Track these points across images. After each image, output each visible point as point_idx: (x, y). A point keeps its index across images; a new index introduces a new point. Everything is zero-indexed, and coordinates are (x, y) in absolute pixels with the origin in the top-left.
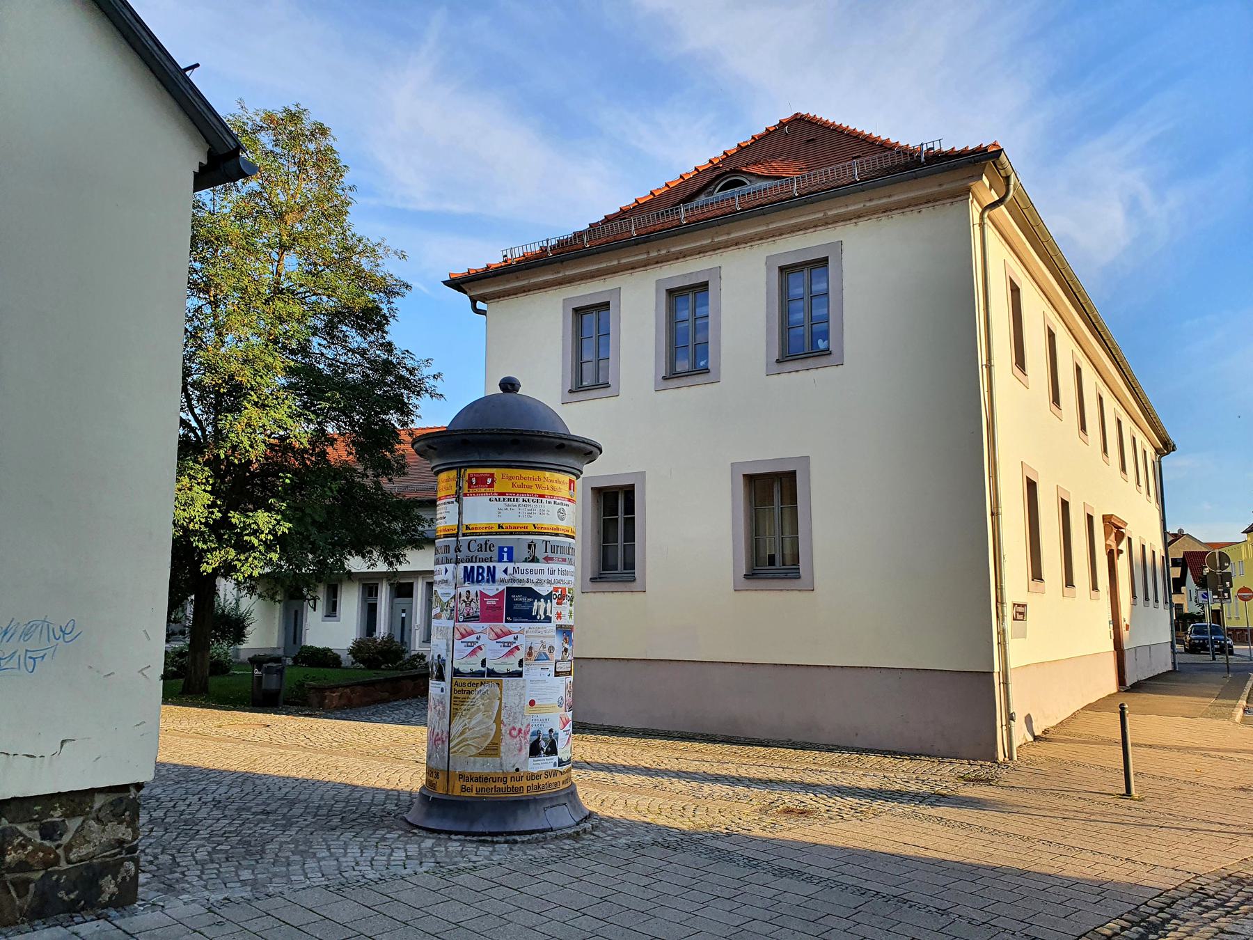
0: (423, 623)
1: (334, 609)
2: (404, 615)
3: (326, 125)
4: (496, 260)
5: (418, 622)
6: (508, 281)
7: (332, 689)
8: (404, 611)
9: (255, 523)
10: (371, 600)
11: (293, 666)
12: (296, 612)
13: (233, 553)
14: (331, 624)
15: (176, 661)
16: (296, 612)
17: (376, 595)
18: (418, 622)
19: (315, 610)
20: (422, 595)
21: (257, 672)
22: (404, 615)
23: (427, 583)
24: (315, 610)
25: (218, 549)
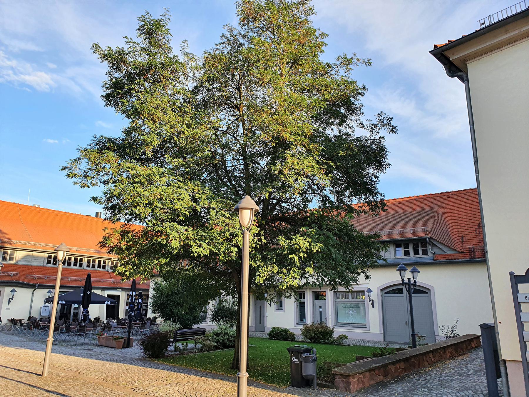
0: (333, 315)
1: (281, 305)
2: (321, 310)
3: (97, 317)
4: (475, 27)
5: (330, 314)
6: (495, 37)
7: (354, 376)
8: (320, 307)
9: (297, 244)
10: (302, 301)
11: (269, 339)
12: (260, 306)
13: (276, 269)
14: (280, 314)
15: (215, 339)
16: (260, 306)
17: (304, 298)
18: (330, 314)
19: (271, 306)
20: (331, 296)
21: (295, 360)
22: (321, 310)
23: (312, 292)
24: (271, 306)
25: (266, 265)
